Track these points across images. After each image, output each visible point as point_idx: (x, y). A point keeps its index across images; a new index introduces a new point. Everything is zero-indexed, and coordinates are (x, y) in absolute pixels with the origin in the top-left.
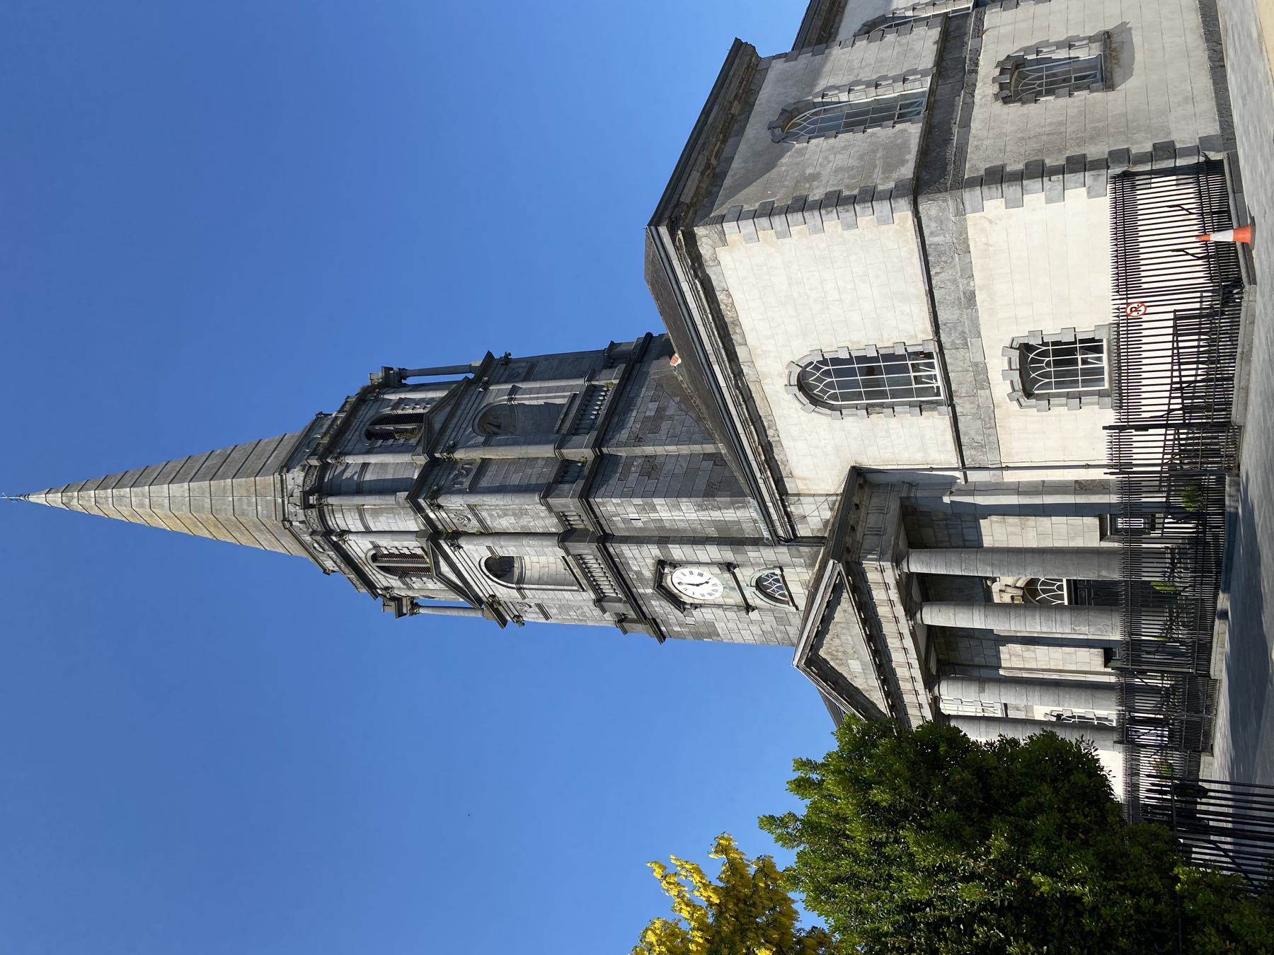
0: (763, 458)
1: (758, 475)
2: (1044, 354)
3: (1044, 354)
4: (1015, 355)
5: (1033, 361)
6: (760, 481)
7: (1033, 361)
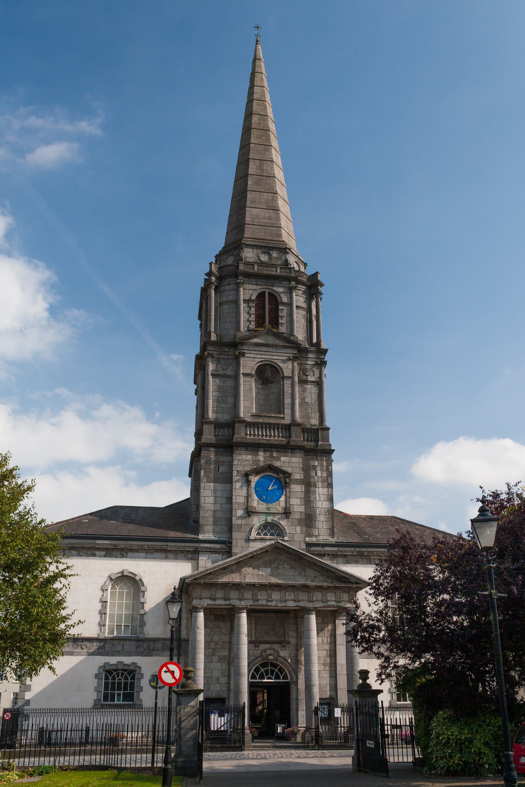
0: (366, 554)
1: (357, 549)
2: (126, 678)
3: (126, 678)
4: (132, 668)
5: (122, 674)
6: (353, 549)
7: (122, 674)
